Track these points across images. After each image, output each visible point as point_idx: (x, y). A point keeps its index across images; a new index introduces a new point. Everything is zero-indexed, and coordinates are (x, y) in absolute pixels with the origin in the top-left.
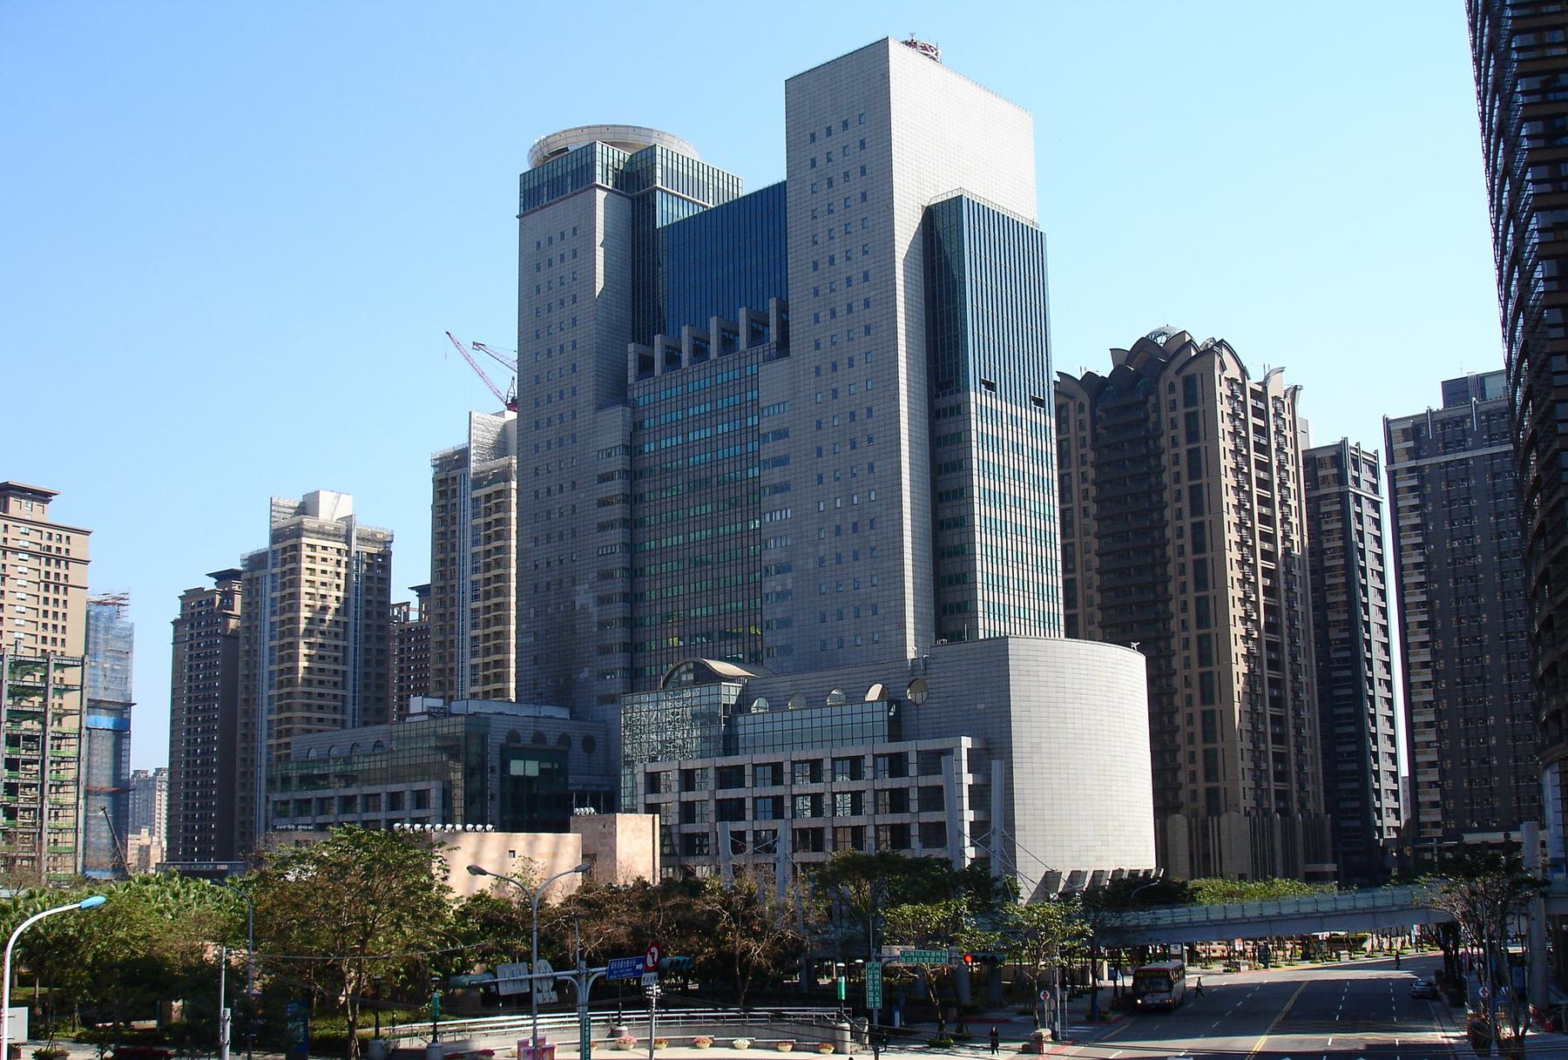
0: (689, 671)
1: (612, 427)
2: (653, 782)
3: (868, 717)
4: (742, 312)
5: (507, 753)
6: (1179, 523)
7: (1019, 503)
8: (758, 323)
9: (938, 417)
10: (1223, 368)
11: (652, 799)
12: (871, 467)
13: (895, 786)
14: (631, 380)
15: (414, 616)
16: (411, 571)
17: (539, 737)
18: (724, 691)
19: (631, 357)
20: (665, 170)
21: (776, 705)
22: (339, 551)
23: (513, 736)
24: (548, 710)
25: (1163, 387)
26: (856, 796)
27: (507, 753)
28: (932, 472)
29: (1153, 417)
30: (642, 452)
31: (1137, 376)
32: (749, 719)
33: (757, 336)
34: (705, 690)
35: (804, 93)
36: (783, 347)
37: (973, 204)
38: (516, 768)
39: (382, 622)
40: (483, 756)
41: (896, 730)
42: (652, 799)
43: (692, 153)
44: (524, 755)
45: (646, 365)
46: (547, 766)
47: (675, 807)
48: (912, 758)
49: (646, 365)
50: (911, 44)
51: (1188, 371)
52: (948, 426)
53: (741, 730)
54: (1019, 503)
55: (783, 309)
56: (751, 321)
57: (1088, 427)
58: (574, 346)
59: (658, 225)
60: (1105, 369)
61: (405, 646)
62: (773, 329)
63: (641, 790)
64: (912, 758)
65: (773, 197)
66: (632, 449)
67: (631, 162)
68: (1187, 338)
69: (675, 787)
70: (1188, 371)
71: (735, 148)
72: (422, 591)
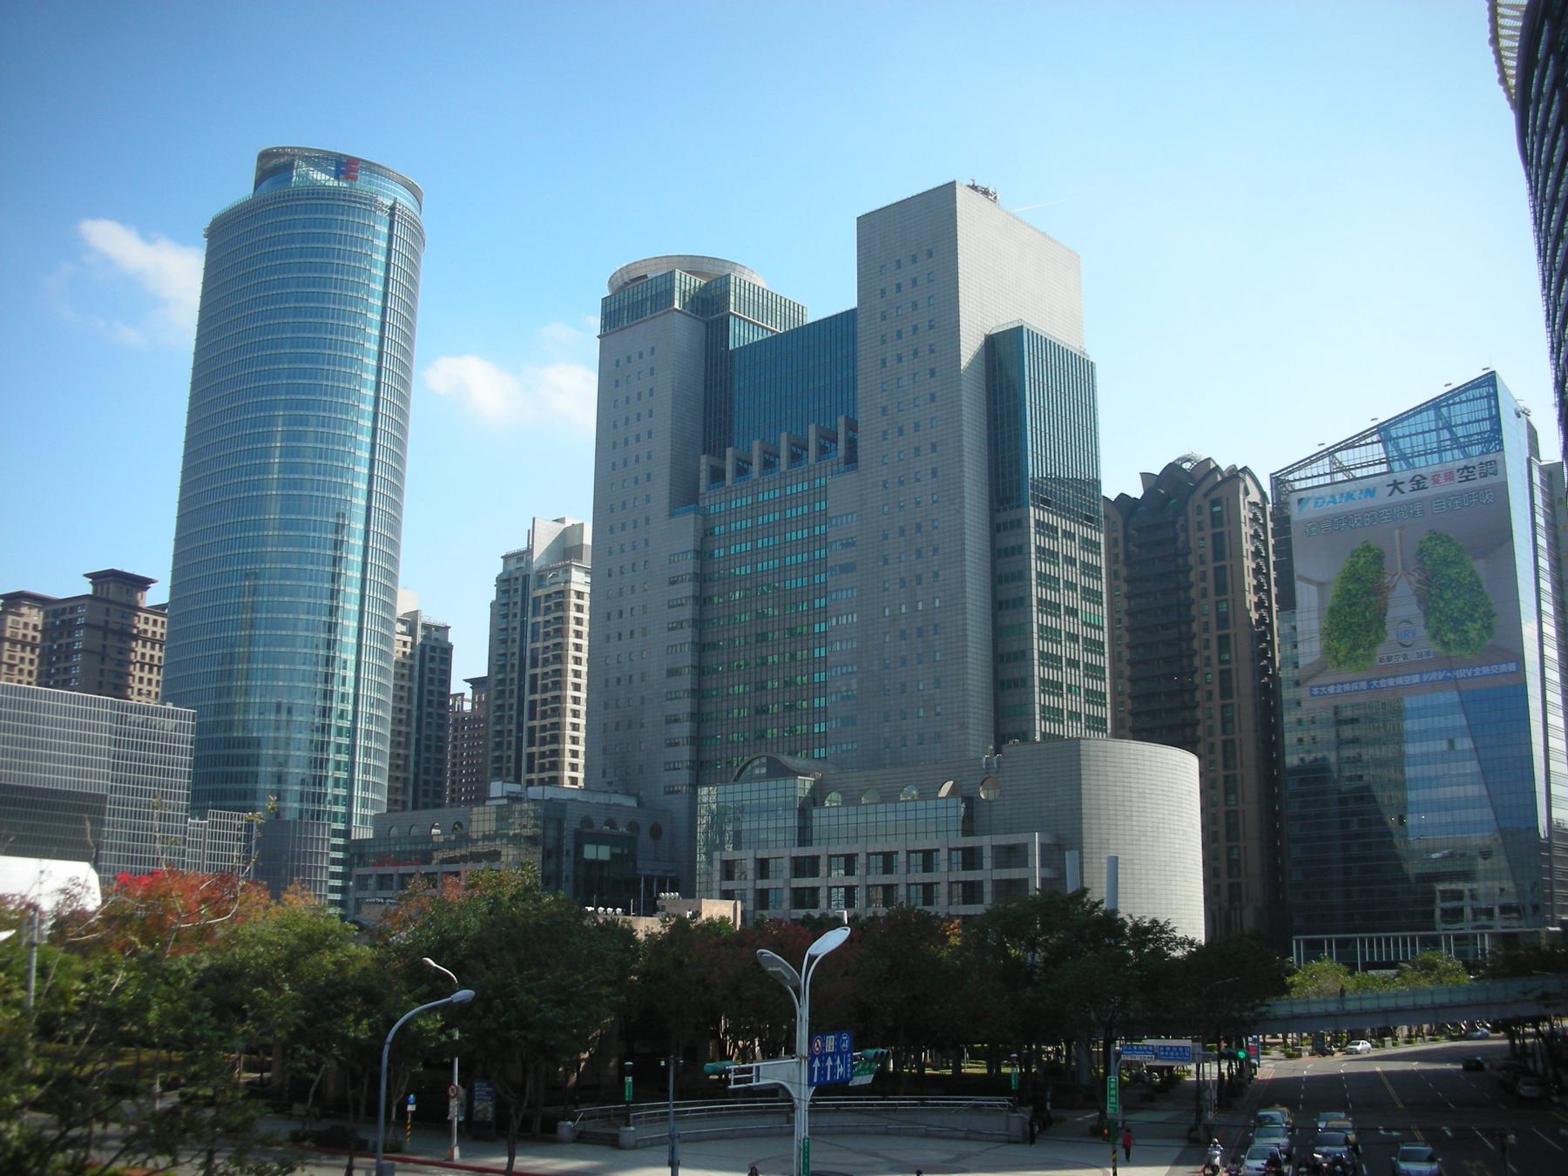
0: (760, 766)
1: (685, 532)
2: (729, 870)
3: (942, 813)
4: (756, 444)
5: (581, 838)
6: (1206, 636)
7: (1072, 612)
8: (798, 447)
9: (999, 530)
10: (1247, 493)
11: (728, 885)
12: (936, 575)
13: (886, 882)
14: (702, 489)
15: (467, 707)
16: (470, 660)
17: (611, 823)
18: (799, 784)
19: (703, 467)
20: (738, 297)
21: (850, 800)
22: (405, 643)
23: (587, 822)
24: (617, 799)
25: (1191, 509)
26: (850, 891)
27: (581, 838)
28: (993, 581)
29: (1182, 537)
30: (712, 556)
31: (1167, 498)
32: (824, 812)
33: (823, 451)
34: (781, 783)
35: (874, 229)
36: (852, 458)
37: (1031, 334)
38: (590, 852)
39: (442, 711)
40: (559, 839)
41: (969, 825)
42: (728, 885)
43: (761, 283)
44: (598, 839)
45: (717, 475)
46: (618, 851)
47: (750, 895)
48: (987, 853)
49: (717, 475)
50: (974, 187)
51: (1215, 495)
52: (1009, 539)
53: (815, 822)
54: (1072, 612)
55: (852, 426)
56: (792, 444)
57: (1121, 545)
58: (649, 457)
59: (731, 347)
60: (1136, 491)
61: (459, 734)
62: (841, 445)
63: (717, 876)
64: (987, 853)
65: (847, 318)
66: (702, 553)
67: (706, 288)
68: (1212, 466)
69: (750, 875)
70: (1215, 495)
71: (808, 275)
72: (476, 683)
